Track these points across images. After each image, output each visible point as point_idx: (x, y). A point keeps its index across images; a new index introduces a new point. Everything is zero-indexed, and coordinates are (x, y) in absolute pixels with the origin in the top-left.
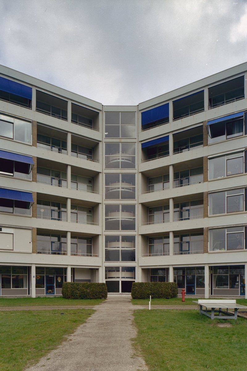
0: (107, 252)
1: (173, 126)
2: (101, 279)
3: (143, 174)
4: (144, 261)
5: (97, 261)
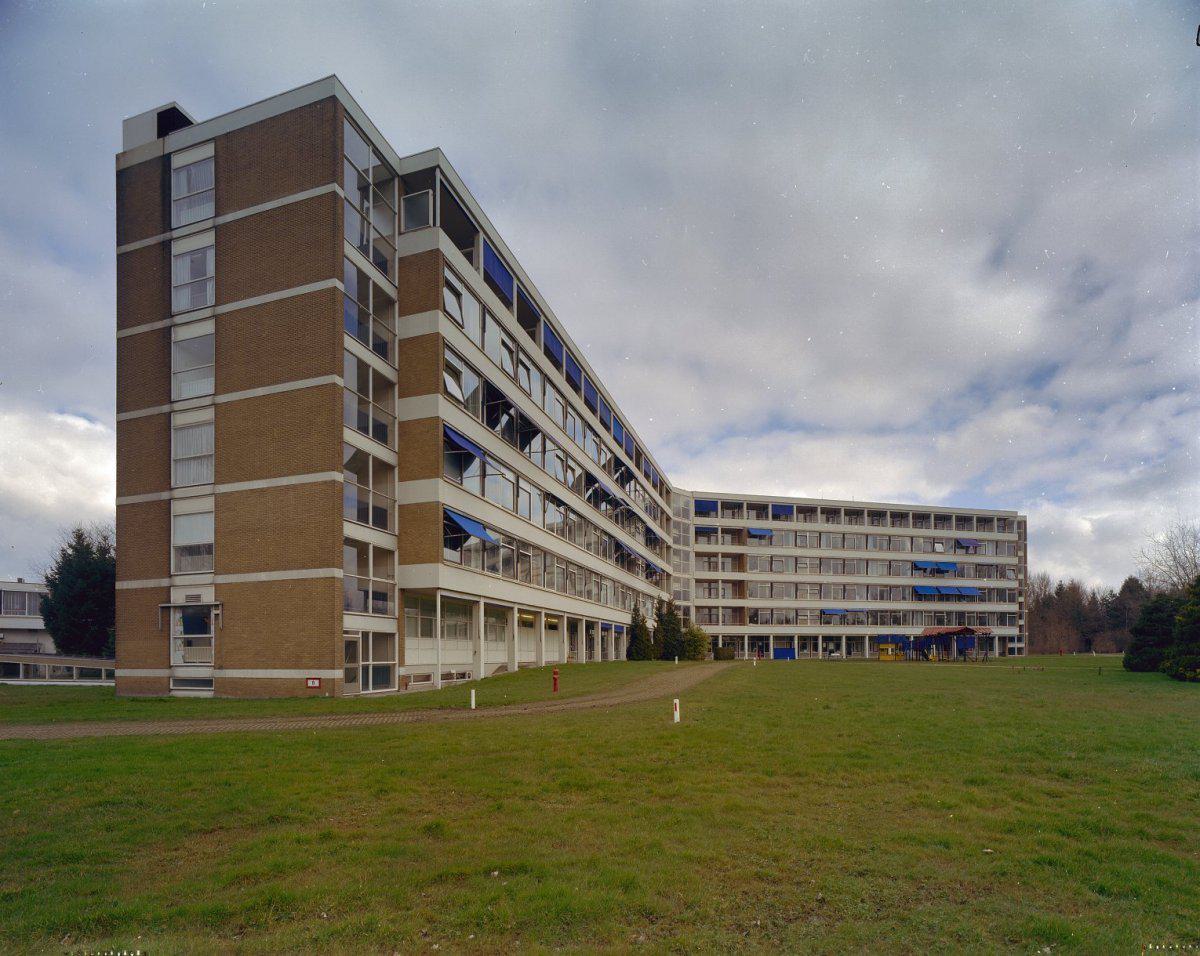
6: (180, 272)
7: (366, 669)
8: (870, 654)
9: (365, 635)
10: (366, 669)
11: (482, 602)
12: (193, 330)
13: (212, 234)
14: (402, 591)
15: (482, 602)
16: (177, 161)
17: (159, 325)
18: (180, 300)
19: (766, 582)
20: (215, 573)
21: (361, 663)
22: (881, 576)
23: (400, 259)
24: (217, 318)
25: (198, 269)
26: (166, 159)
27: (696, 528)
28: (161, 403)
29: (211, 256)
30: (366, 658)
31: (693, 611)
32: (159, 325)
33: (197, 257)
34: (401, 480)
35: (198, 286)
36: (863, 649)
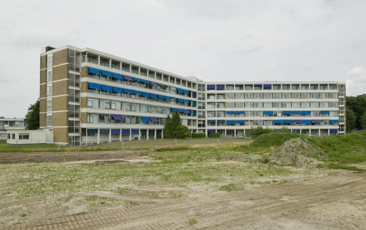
0: (198, 115)
1: (216, 92)
2: (197, 132)
3: (208, 120)
4: (208, 127)
5: (196, 127)
6: (48, 89)
7: (73, 143)
8: (330, 135)
9: (73, 137)
10: (73, 143)
11: (163, 74)
12: (50, 84)
13: (52, 69)
14: (81, 128)
15: (163, 74)
16: (48, 56)
17: (45, 83)
18: (48, 93)
19: (280, 93)
20: (52, 111)
21: (72, 142)
22: (316, 107)
23: (81, 68)
24: (53, 83)
25: (50, 90)
26: (46, 56)
27: (207, 85)
28: (45, 97)
29: (52, 72)
30: (73, 141)
31: (206, 112)
32: (45, 83)
33: (50, 87)
34: (81, 108)
35: (50, 92)
36: (309, 134)
